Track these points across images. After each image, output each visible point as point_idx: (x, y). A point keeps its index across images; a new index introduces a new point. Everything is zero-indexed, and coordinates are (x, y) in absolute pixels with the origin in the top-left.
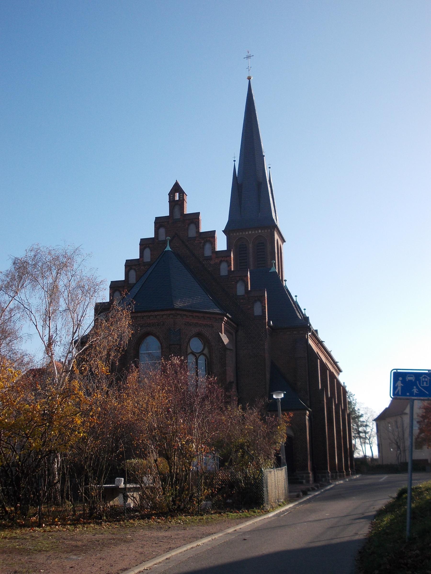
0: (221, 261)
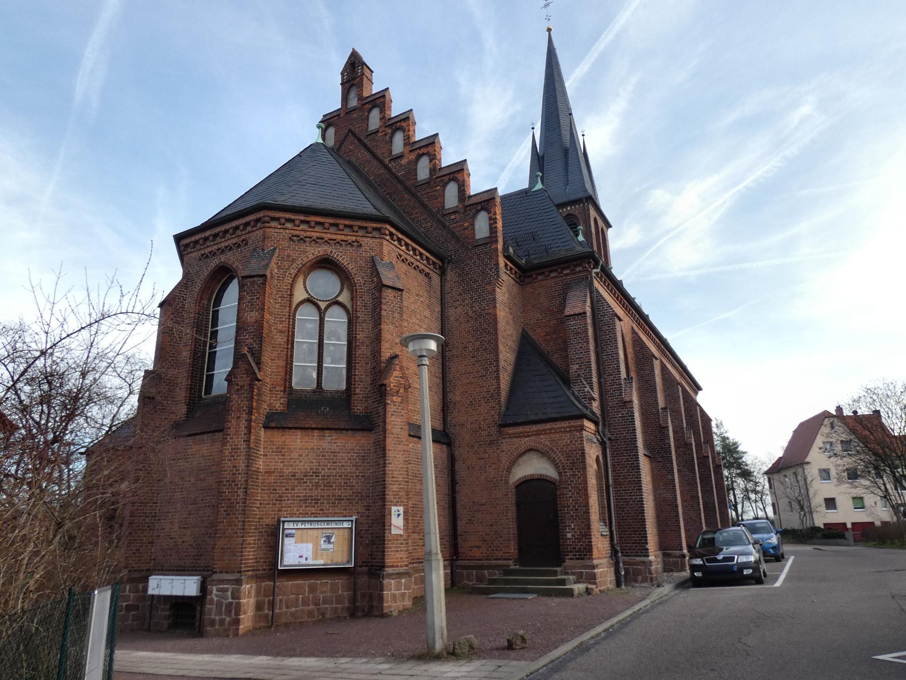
0: (419, 156)
